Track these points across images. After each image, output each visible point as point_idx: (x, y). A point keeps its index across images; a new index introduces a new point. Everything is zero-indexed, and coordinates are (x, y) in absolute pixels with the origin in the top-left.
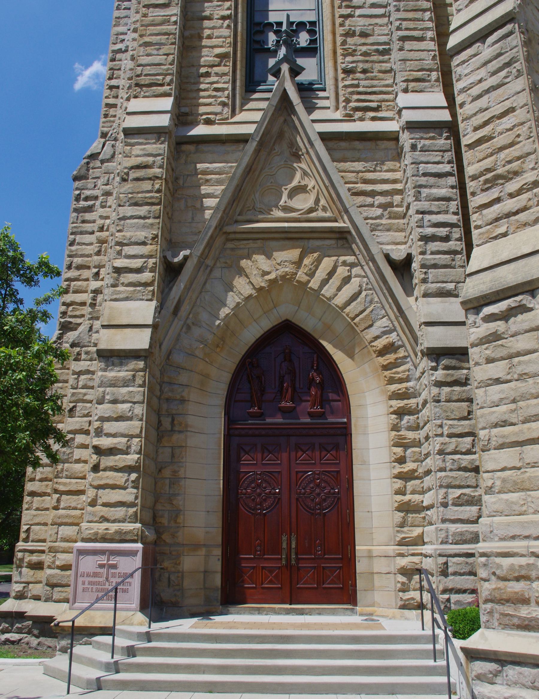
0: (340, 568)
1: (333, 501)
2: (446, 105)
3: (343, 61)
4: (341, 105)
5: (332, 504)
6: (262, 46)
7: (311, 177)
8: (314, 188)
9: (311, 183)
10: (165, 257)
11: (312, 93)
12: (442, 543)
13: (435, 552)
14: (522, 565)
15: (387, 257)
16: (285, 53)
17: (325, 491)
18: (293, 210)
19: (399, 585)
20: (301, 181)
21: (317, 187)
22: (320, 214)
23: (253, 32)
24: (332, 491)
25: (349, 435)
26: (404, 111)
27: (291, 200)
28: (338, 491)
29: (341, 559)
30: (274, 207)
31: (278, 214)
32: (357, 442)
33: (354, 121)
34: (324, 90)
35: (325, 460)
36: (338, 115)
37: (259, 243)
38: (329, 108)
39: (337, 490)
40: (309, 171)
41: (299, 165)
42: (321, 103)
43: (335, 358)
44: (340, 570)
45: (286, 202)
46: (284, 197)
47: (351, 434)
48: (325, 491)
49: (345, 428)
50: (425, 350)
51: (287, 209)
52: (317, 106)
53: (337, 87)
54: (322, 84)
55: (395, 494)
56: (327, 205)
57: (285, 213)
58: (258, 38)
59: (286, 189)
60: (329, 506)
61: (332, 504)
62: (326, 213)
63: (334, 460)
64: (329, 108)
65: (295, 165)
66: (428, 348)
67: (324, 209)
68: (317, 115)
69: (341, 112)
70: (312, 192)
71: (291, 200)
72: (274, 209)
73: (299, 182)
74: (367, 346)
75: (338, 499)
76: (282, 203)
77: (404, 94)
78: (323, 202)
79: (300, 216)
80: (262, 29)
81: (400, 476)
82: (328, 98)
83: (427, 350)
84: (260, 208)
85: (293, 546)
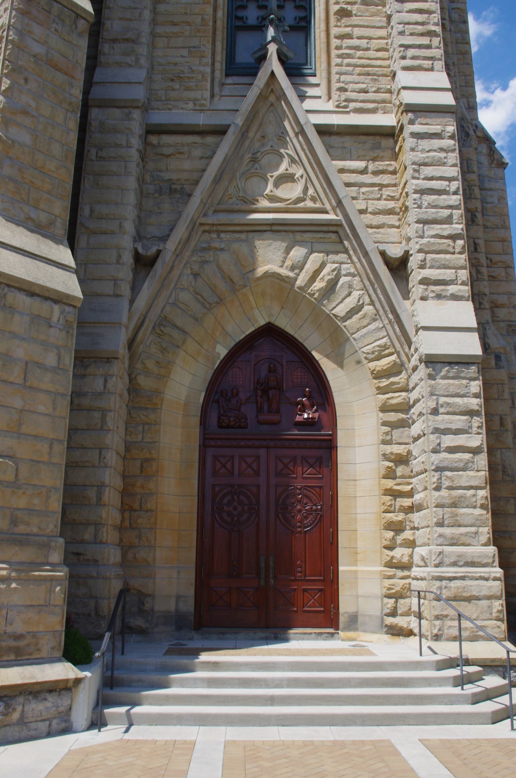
0: (320, 590)
1: (316, 518)
2: (449, 86)
3: (388, 438)
4: (335, 95)
5: (314, 522)
6: (244, 23)
7: (299, 165)
8: (302, 177)
9: (299, 172)
10: (136, 250)
11: (302, 78)
12: (436, 566)
13: (429, 575)
14: (341, 169)
15: (383, 254)
16: (273, 34)
17: (306, 508)
18: (281, 200)
19: (384, 590)
20: (289, 169)
21: (305, 175)
22: (309, 204)
23: (234, 7)
24: (314, 507)
25: (335, 448)
26: (402, 90)
27: (277, 189)
28: (321, 508)
29: (323, 581)
30: (260, 196)
31: (264, 203)
32: (342, 456)
33: (348, 113)
34: (314, 75)
35: (307, 474)
36: (330, 106)
37: (243, 236)
38: (320, 97)
39: (319, 507)
40: (296, 158)
41: (287, 151)
42: (311, 91)
43: (320, 362)
44: (322, 593)
45: (271, 191)
46: (270, 187)
47: (337, 447)
48: (306, 508)
49: (330, 440)
50: (423, 357)
51: (272, 199)
52: (307, 95)
53: (329, 73)
54: (311, 69)
55: (383, 478)
56: (315, 195)
57: (271, 203)
58: (240, 14)
59: (272, 177)
60: (311, 524)
61: (314, 522)
62: (315, 203)
63: (316, 474)
64: (320, 97)
65: (282, 151)
66: (426, 355)
67: (313, 199)
68: (308, 104)
69: (333, 102)
70: (299, 180)
71: (277, 189)
72: (259, 198)
73: (287, 170)
74: (357, 351)
75: (321, 516)
76: (267, 191)
77: (404, 71)
78: (311, 191)
79: (286, 206)
80: (245, 3)
81: (389, 492)
82: (318, 85)
83: (425, 357)
84: (243, 197)
85: (271, 564)
